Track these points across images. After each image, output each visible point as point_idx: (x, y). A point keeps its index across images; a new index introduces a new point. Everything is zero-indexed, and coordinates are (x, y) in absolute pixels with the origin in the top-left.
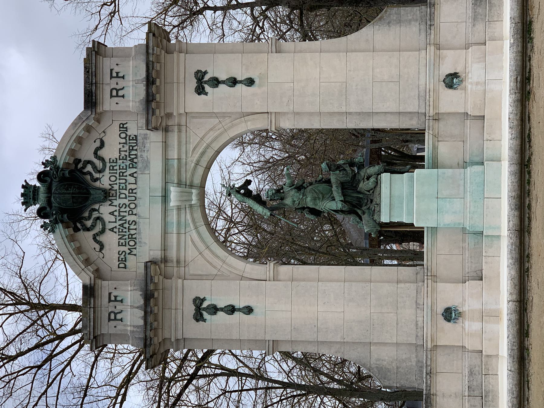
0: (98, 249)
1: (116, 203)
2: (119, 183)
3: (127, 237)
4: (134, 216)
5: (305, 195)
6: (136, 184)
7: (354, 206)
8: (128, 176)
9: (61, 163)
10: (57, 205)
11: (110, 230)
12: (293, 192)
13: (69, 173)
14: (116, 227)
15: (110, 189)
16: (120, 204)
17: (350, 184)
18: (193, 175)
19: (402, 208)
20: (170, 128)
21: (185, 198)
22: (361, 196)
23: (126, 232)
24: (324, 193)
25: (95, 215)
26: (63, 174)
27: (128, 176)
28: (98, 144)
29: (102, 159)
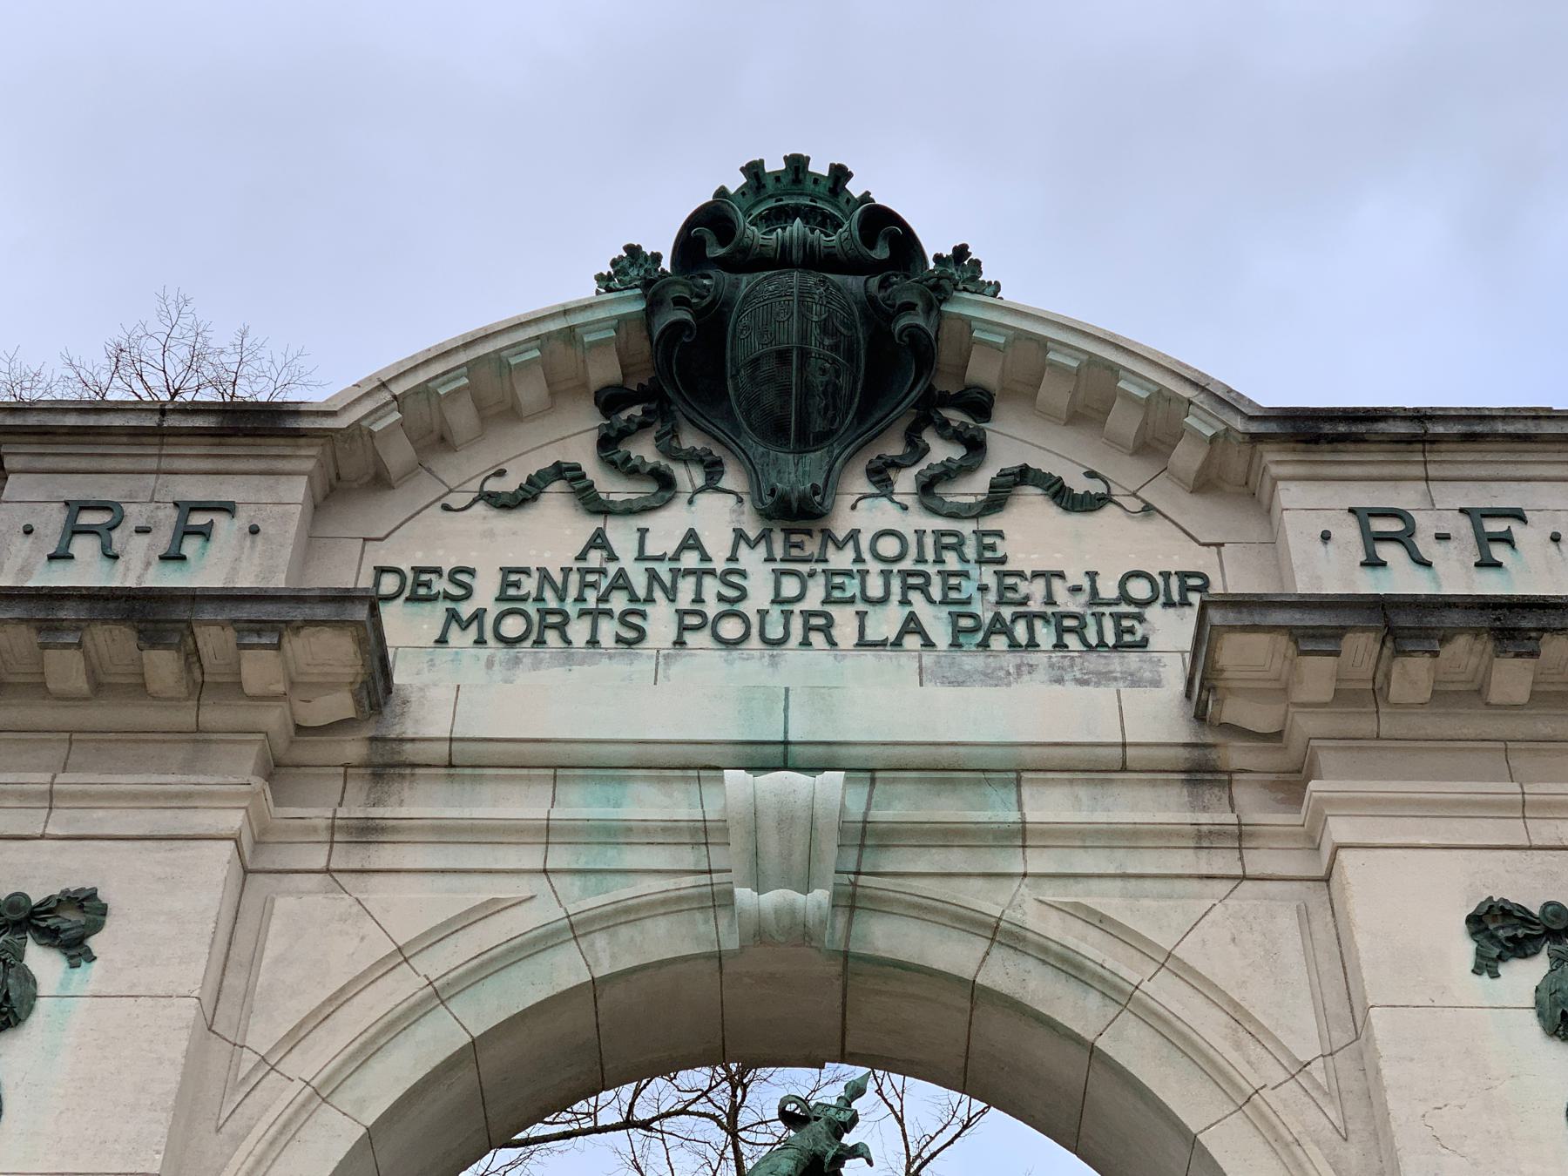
0: (493, 486)
1: (751, 559)
2: (864, 574)
3: (552, 603)
4: (673, 636)
6: (863, 643)
8: (907, 610)
9: (963, 306)
10: (743, 289)
11: (600, 534)
13: (914, 332)
14: (613, 558)
15: (828, 535)
16: (743, 574)
18: (924, 911)
20: (1210, 795)
21: (771, 845)
23: (580, 599)
25: (687, 477)
26: (909, 307)
27: (907, 610)
28: (1079, 484)
29: (997, 500)
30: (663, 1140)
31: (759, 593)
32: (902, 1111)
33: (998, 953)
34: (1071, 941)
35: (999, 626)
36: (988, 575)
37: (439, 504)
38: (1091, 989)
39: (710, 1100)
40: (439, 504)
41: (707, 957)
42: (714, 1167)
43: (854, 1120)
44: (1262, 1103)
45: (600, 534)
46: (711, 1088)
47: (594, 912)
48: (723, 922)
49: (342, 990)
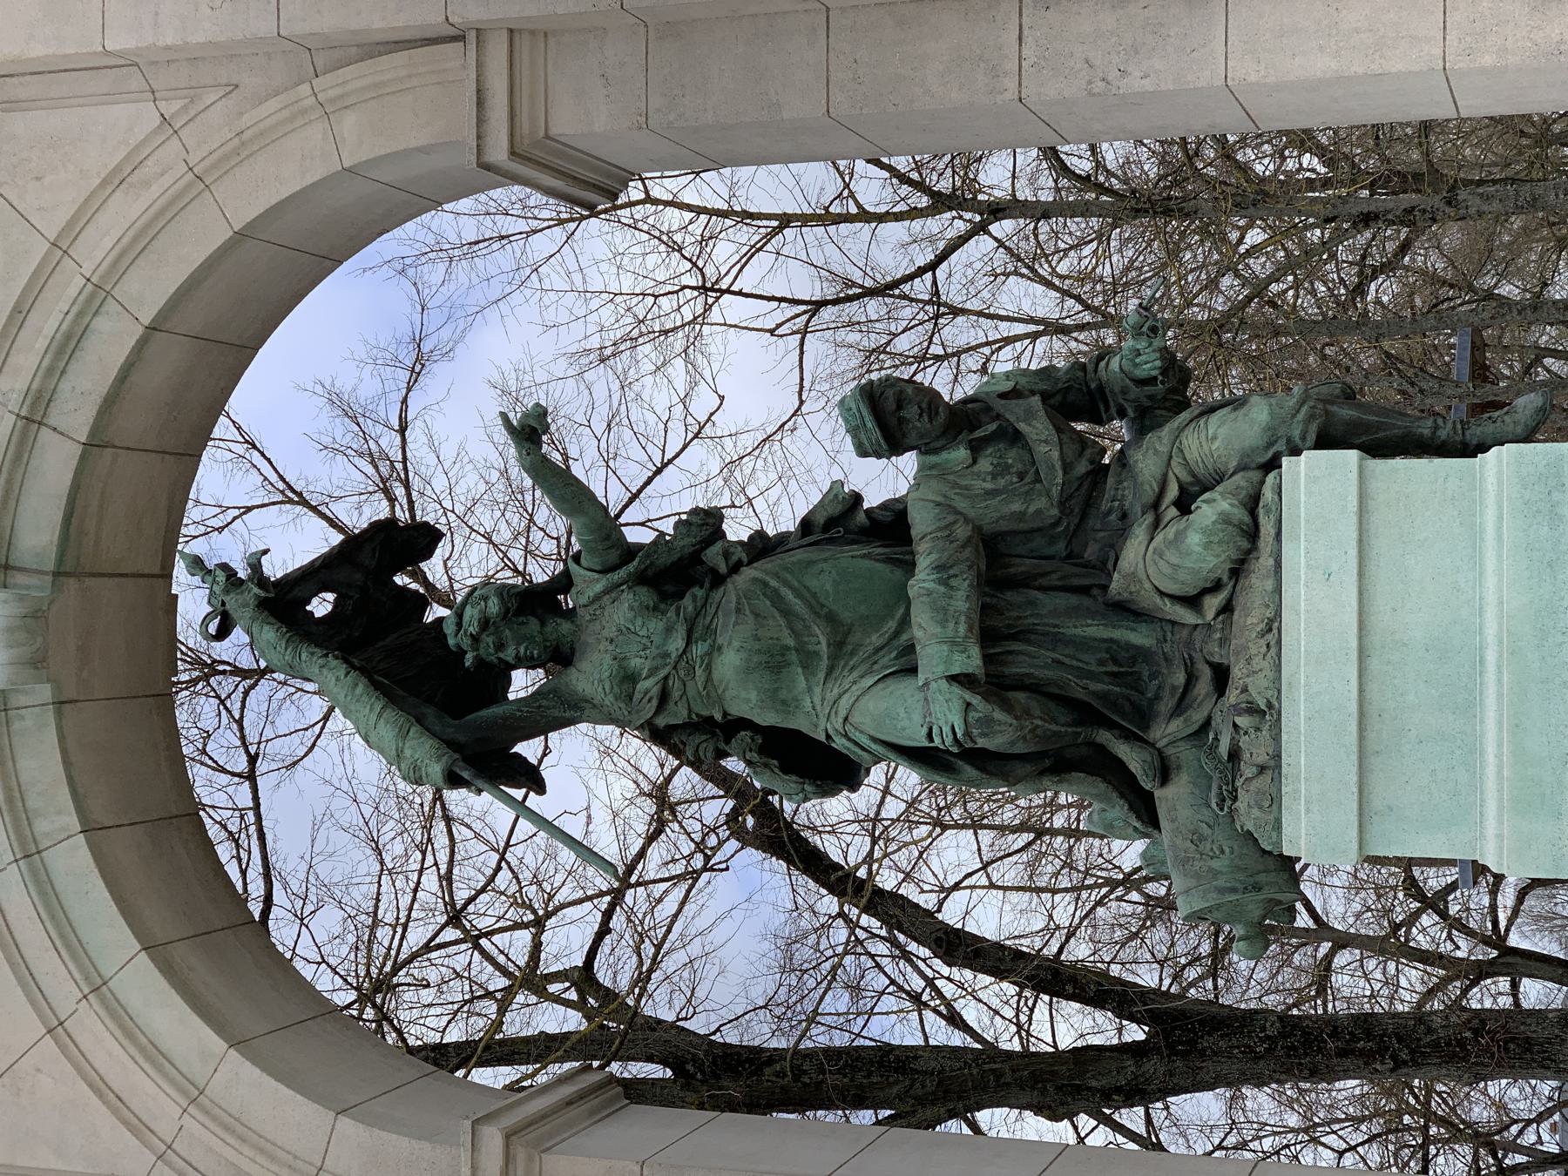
5: (710, 631)
7: (1085, 713)
12: (622, 611)
17: (1060, 547)
19: (1474, 750)
22: (1140, 637)
24: (846, 616)
30: (267, 741)
32: (239, 508)
33: (52, 420)
34: (41, 344)
38: (91, 326)
39: (229, 696)
41: (59, 715)
42: (293, 690)
43: (224, 567)
44: (202, 165)
46: (218, 697)
47: (12, 837)
48: (23, 700)
49: (91, 1085)
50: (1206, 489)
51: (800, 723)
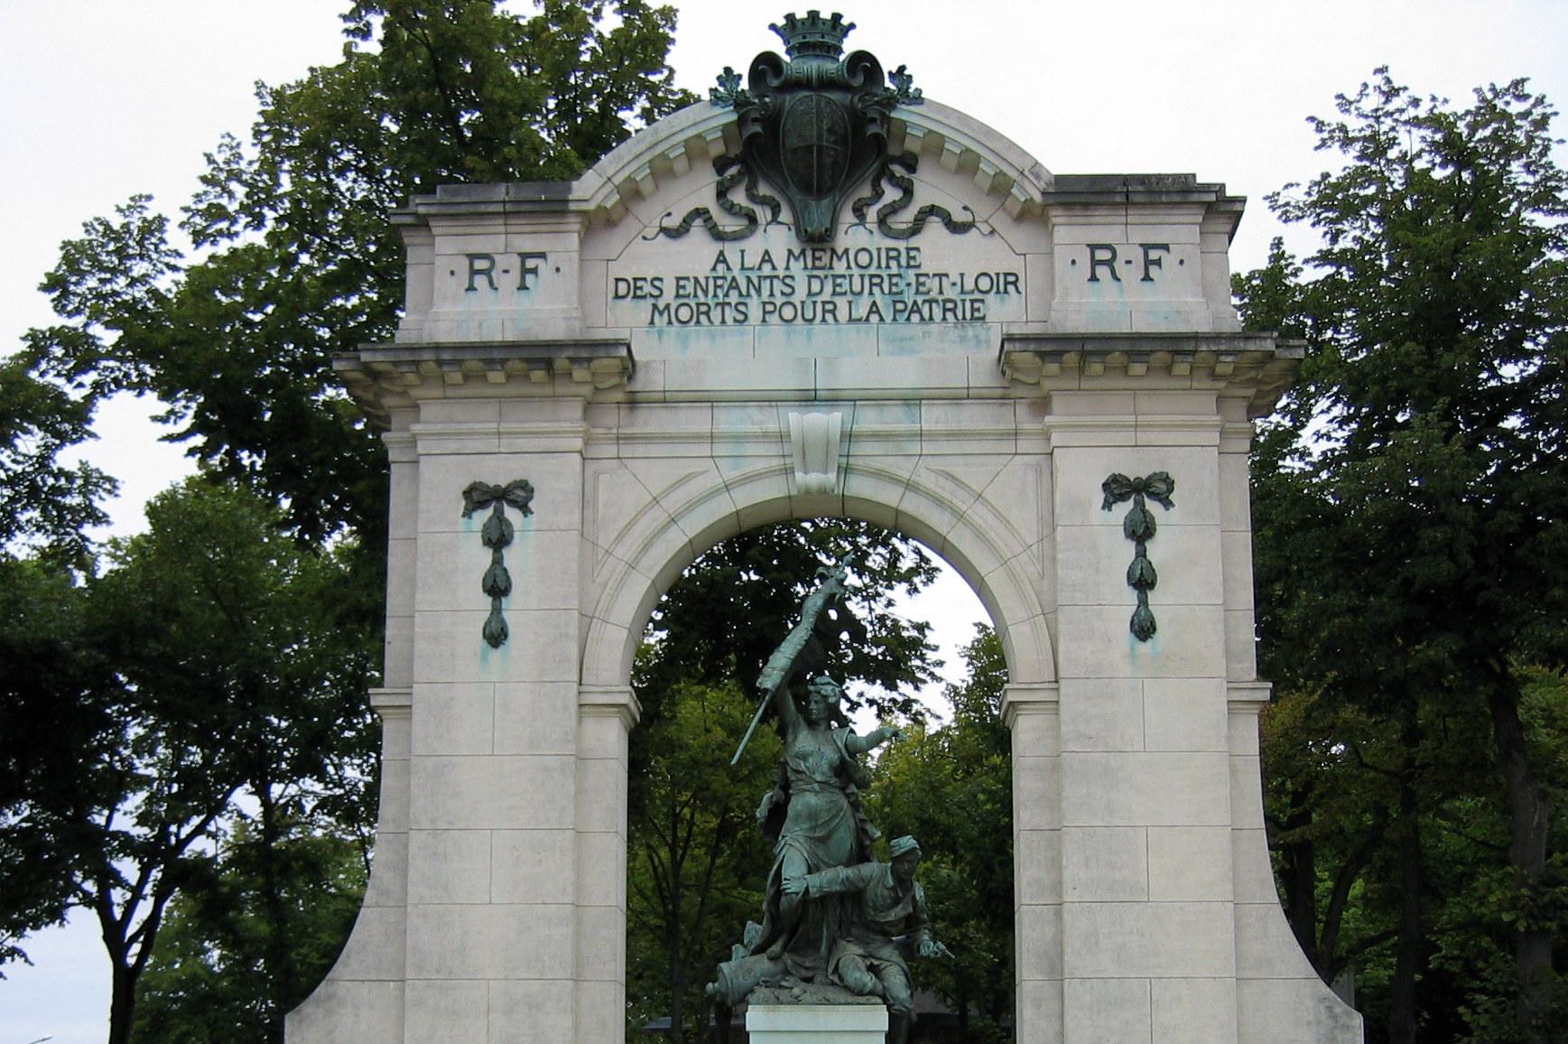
0: (667, 223)
2: (851, 276)
3: (702, 299)
5: (823, 790)
9: (902, 113)
11: (721, 253)
12: (831, 755)
13: (876, 136)
14: (729, 268)
15: (833, 251)
16: (792, 278)
18: (878, 474)
22: (823, 948)
23: (715, 295)
26: (873, 120)
28: (959, 216)
29: (916, 229)
31: (800, 294)
35: (916, 309)
36: (911, 275)
37: (640, 236)
40: (640, 236)
45: (721, 253)
50: (876, 976)
51: (788, 824)
